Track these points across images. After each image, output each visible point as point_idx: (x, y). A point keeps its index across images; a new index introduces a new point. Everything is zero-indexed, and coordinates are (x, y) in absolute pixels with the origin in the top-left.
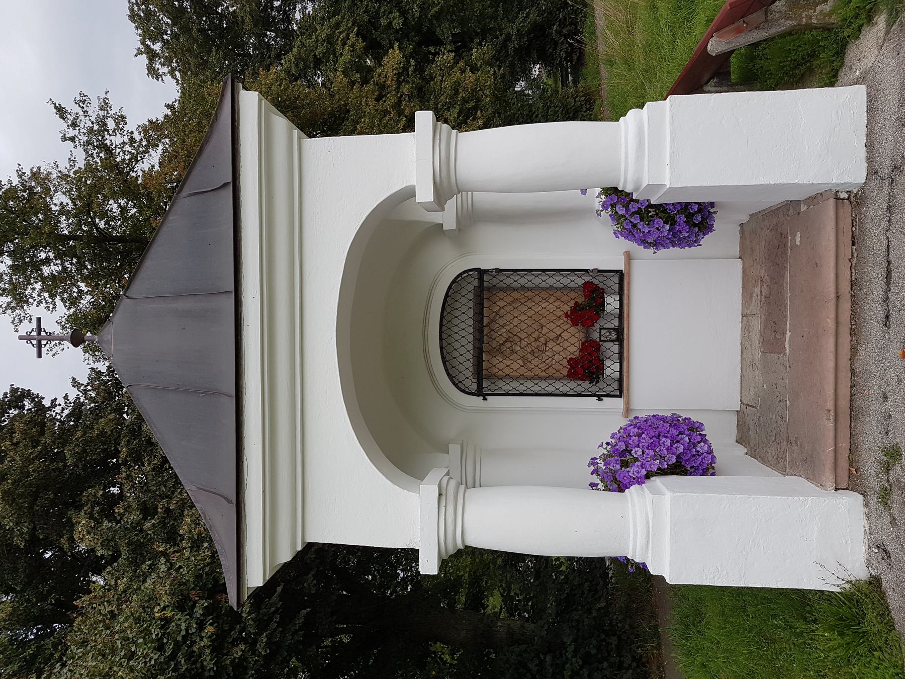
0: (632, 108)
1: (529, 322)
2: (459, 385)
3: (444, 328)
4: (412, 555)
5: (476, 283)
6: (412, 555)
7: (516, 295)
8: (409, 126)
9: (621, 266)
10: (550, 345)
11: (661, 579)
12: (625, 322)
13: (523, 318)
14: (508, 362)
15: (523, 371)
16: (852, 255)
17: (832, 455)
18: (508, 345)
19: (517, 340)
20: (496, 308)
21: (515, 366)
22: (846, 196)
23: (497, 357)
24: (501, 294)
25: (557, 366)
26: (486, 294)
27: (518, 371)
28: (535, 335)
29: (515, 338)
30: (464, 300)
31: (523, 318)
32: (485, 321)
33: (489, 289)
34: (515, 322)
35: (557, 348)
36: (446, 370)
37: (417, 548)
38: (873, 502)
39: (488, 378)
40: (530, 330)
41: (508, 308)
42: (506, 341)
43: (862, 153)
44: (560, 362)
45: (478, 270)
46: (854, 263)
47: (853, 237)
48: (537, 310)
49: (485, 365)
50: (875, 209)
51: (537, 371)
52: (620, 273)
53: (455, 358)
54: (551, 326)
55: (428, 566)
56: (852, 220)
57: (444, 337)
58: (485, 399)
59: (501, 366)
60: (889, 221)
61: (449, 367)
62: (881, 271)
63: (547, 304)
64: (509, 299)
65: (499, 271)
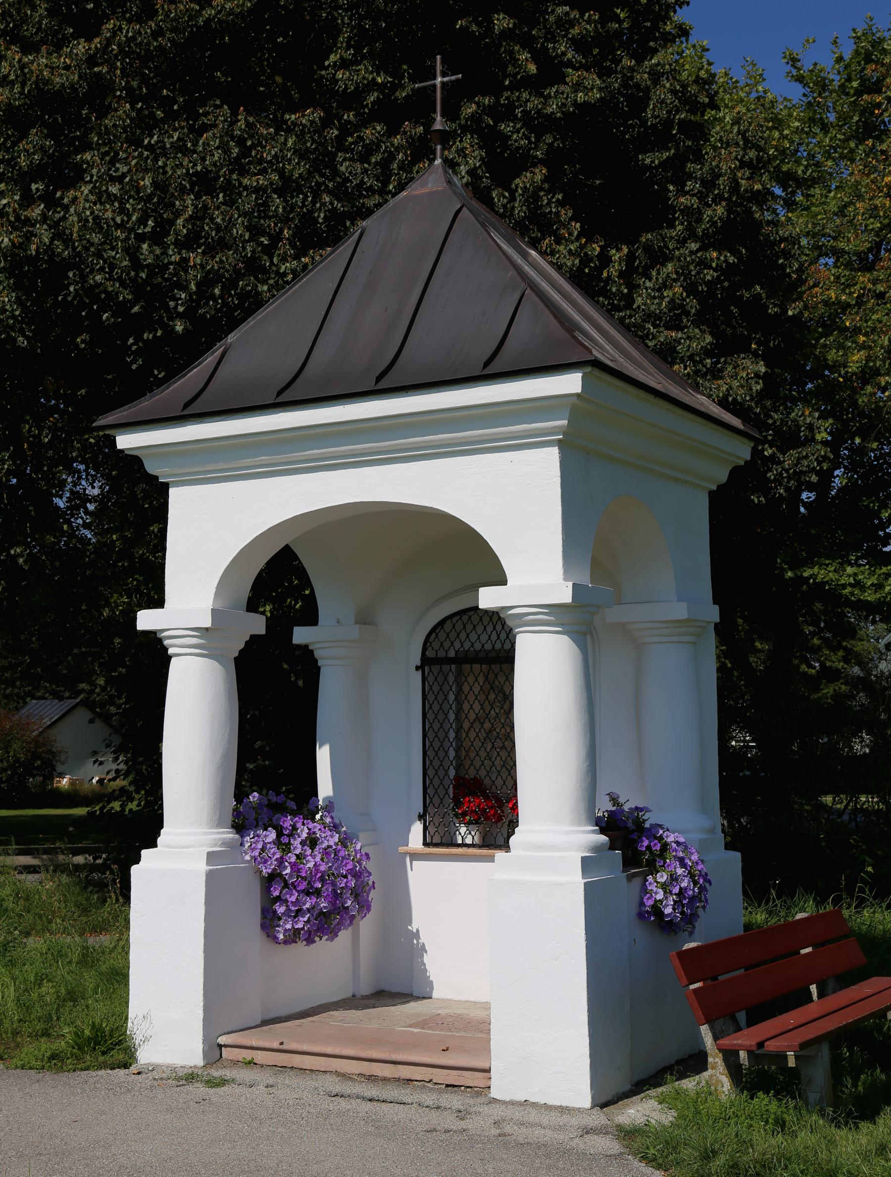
2: (433, 635)
4: (158, 602)
6: (158, 602)
11: (137, 860)
16: (436, 1084)
39: (460, 672)
46: (429, 1085)
47: (454, 1086)
48: (481, 753)
55: (146, 620)
56: (471, 1087)
58: (417, 668)
61: (455, 619)
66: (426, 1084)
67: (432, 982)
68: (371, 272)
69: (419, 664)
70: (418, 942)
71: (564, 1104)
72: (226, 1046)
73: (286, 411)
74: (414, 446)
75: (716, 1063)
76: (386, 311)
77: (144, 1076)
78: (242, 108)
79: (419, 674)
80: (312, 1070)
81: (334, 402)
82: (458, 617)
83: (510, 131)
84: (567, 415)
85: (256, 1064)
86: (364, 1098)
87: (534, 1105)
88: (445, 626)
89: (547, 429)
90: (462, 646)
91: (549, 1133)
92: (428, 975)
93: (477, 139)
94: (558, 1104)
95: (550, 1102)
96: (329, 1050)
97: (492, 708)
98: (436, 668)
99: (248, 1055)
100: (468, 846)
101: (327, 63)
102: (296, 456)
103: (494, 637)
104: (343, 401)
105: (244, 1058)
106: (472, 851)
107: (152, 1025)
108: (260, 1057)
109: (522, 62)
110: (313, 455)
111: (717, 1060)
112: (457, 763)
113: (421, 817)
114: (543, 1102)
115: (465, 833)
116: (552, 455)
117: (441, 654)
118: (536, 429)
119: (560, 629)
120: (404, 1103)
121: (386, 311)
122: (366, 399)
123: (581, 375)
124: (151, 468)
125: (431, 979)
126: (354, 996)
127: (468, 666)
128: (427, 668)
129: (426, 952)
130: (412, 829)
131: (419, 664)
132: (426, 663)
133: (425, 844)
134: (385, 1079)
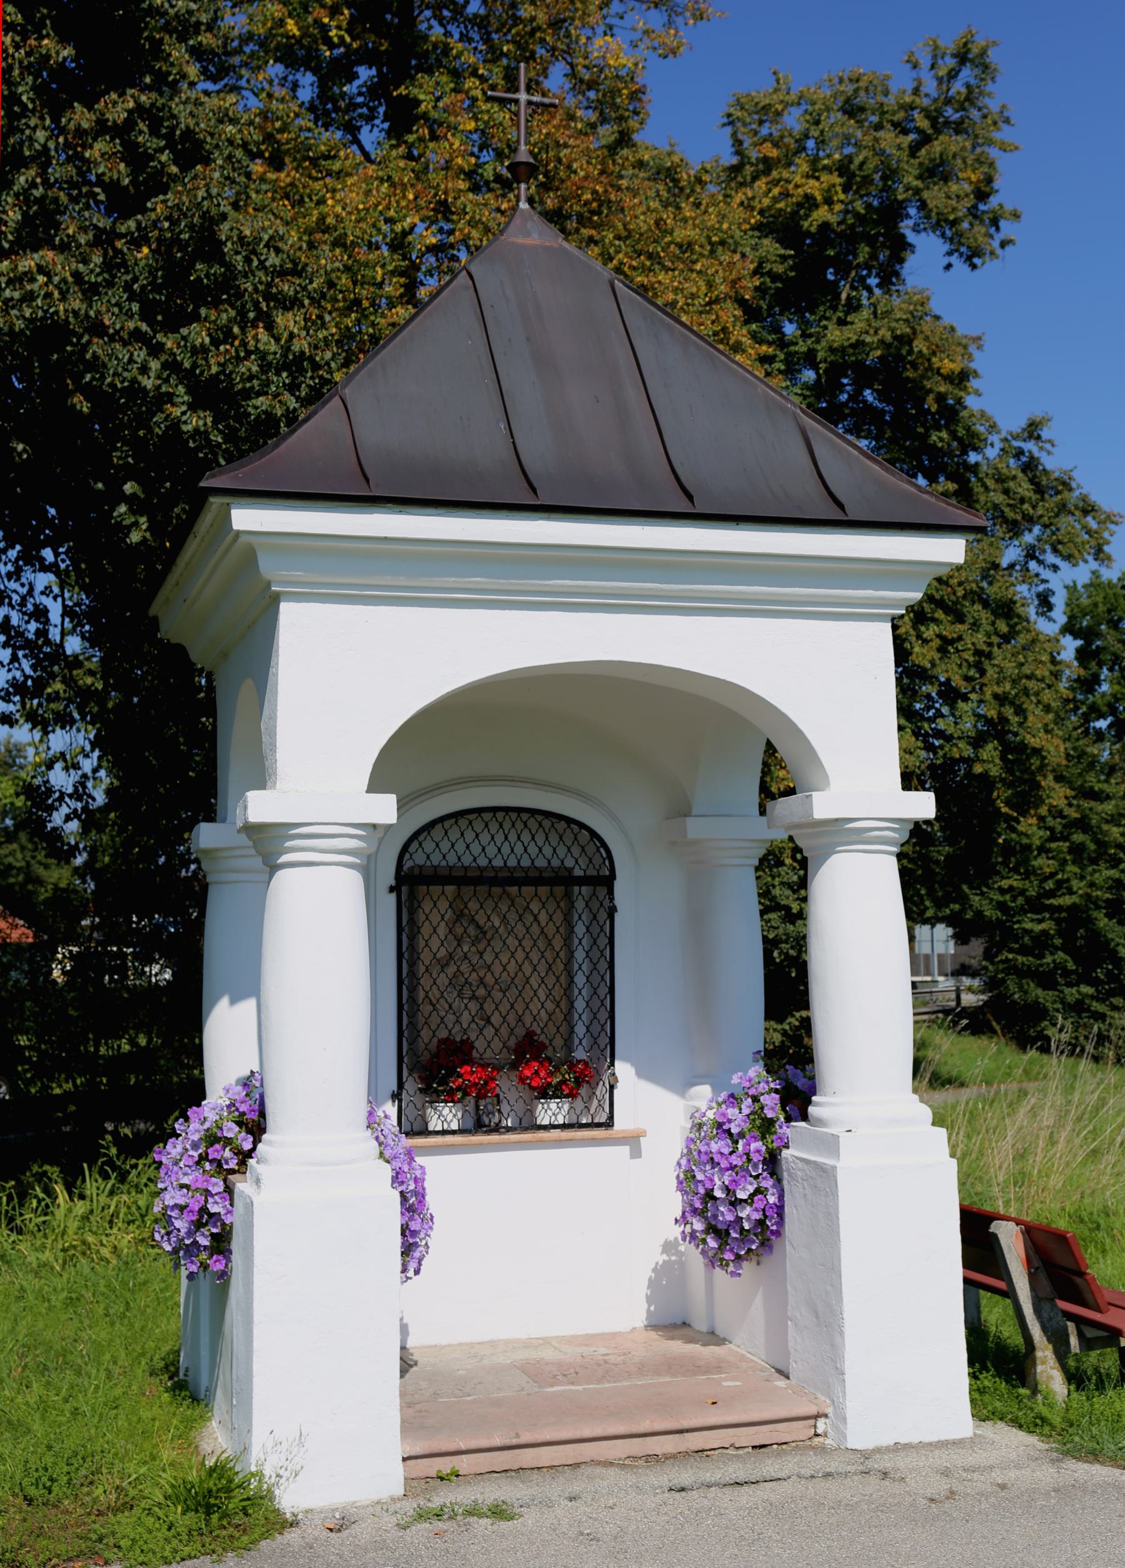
0: (930, 1106)
1: (512, 967)
2: (415, 845)
3: (514, 815)
5: (578, 872)
7: (558, 943)
8: (910, 780)
9: (619, 1123)
10: (473, 1006)
12: (530, 1135)
13: (520, 955)
14: (442, 930)
15: (426, 957)
17: (452, 1447)
18: (472, 931)
19: (481, 947)
20: (535, 907)
21: (435, 944)
22: (819, 1431)
23: (449, 911)
24: (558, 917)
25: (434, 1020)
26: (559, 890)
27: (426, 949)
28: (489, 979)
29: (484, 942)
30: (562, 851)
31: (520, 955)
32: (514, 890)
33: (568, 895)
34: (512, 942)
35: (466, 1018)
36: (441, 820)
37: (278, 785)
38: (410, 1506)
40: (497, 969)
41: (535, 930)
42: (478, 927)
43: (887, 1441)
44: (442, 1025)
45: (613, 876)
49: (436, 889)
50: (814, 1463)
51: (426, 982)
52: (609, 1123)
53: (462, 834)
54: (504, 1007)
57: (522, 815)
59: (435, 918)
60: (813, 1477)
61: (447, 824)
62: (741, 1476)
63: (543, 998)
64: (550, 930)
65: (612, 912)
71: (943, 1438)
73: (548, 519)
74: (582, 590)
79: (393, 897)
81: (762, 527)
82: (453, 821)
87: (908, 1446)
88: (433, 833)
89: (895, 599)
93: (121, 145)
96: (587, 1433)
99: (444, 1465)
100: (453, 1132)
103: (506, 849)
104: (561, 516)
106: (555, 1134)
108: (464, 1464)
110: (562, 586)
112: (572, 1017)
113: (396, 1096)
117: (591, 872)
118: (881, 598)
119: (363, 833)
122: (798, 529)
127: (576, 889)
128: (404, 889)
131: (393, 883)
134: (669, 1457)
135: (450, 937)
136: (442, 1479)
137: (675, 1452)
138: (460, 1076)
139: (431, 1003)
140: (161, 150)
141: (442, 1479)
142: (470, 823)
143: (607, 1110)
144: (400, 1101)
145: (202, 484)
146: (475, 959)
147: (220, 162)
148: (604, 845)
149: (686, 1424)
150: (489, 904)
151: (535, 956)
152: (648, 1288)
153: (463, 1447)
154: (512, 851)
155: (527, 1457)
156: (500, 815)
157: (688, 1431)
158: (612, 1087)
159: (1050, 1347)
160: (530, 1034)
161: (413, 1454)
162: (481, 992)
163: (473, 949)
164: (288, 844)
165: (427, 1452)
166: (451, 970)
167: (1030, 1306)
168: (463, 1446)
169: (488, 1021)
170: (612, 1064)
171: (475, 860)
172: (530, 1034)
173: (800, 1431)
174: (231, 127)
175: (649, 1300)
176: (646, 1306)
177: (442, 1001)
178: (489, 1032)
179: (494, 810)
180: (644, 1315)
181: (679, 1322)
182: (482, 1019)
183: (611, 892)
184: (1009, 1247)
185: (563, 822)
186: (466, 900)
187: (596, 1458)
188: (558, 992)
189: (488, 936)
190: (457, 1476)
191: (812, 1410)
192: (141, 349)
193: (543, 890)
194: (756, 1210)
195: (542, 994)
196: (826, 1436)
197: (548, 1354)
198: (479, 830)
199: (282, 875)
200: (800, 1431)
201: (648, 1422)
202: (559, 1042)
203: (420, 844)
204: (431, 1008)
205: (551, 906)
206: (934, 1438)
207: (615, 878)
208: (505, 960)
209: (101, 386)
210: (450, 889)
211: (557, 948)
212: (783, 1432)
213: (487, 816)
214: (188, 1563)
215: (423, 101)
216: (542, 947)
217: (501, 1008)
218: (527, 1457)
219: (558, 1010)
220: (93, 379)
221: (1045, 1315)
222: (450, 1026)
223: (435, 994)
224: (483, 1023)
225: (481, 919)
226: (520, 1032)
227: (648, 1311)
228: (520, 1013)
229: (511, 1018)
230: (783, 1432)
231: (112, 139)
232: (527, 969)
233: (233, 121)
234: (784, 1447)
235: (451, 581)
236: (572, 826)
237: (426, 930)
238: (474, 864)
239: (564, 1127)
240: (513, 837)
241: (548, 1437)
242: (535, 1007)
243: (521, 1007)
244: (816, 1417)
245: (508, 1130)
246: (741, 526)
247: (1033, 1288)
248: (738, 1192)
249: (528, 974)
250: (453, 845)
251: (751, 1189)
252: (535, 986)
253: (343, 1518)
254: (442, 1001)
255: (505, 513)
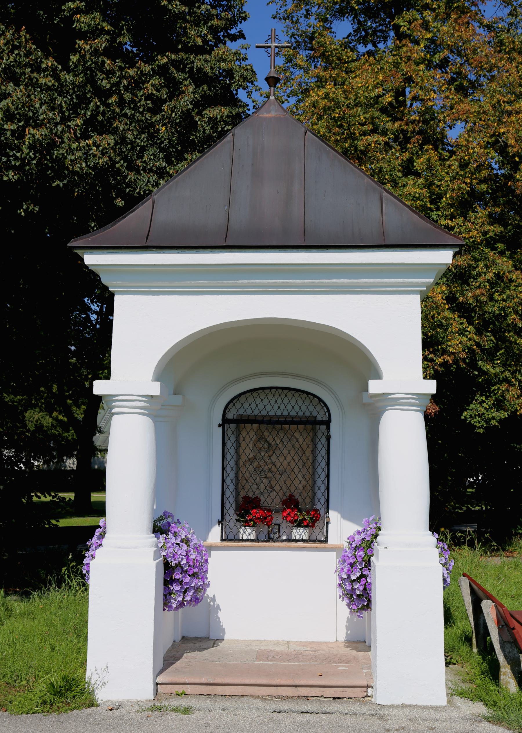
1: (285, 464)
2: (232, 404)
3: (280, 391)
5: (319, 418)
7: (308, 452)
10: (266, 481)
13: (289, 458)
14: (251, 445)
15: (243, 458)
17: (182, 681)
19: (270, 453)
20: (297, 435)
22: (369, 694)
23: (255, 437)
24: (308, 440)
25: (247, 487)
26: (309, 427)
28: (274, 469)
30: (311, 408)
31: (289, 458)
32: (287, 426)
34: (285, 452)
35: (262, 487)
36: (244, 393)
45: (329, 420)
47: (339, 698)
49: (249, 426)
52: (326, 541)
54: (281, 482)
59: (248, 440)
60: (347, 714)
61: (247, 395)
63: (300, 478)
64: (305, 446)
66: (318, 698)
67: (224, 629)
68: (252, 165)
69: (221, 423)
70: (214, 604)
71: (429, 704)
72: (161, 684)
73: (231, 252)
75: (506, 671)
76: (278, 193)
77: (113, 711)
78: (24, 27)
80: (231, 696)
82: (250, 393)
83: (181, 78)
84: (434, 275)
85: (186, 694)
86: (297, 712)
89: (418, 283)
90: (253, 412)
91: (448, 724)
92: (221, 624)
93: (164, 80)
94: (425, 704)
95: (420, 704)
96: (247, 682)
97: (274, 452)
98: (233, 426)
99: (180, 689)
101: (63, 7)
102: (202, 283)
103: (276, 407)
105: (177, 691)
106: (301, 544)
107: (108, 674)
108: (189, 689)
109: (192, 35)
111: (507, 669)
113: (220, 522)
114: (414, 704)
115: (247, 532)
116: (416, 300)
118: (410, 283)
120: (329, 713)
121: (278, 193)
122: (359, 250)
123: (452, 252)
124: (105, 281)
125: (223, 627)
126: (174, 642)
129: (220, 610)
130: (212, 530)
131: (221, 423)
132: (225, 422)
133: (222, 540)
134: (288, 698)
135: (255, 448)
136: (178, 695)
137: (292, 695)
138: (251, 514)
139: (246, 479)
140: (186, 79)
141: (178, 695)
142: (259, 394)
143: (325, 534)
144: (222, 525)
145: (69, 245)
146: (266, 459)
147: (237, 78)
148: (326, 405)
149: (297, 683)
150: (274, 433)
151: (296, 459)
152: (347, 622)
153: (187, 682)
154: (279, 408)
155: (219, 690)
156: (273, 391)
157: (299, 686)
158: (327, 523)
159: (509, 667)
160: (291, 496)
161: (163, 682)
162: (270, 475)
163: (266, 454)
164: (114, 404)
165: (170, 682)
166: (256, 464)
167: (499, 645)
168: (187, 681)
169: (273, 488)
170: (328, 512)
171: (260, 412)
172: (291, 496)
173: (359, 693)
174: (223, 63)
175: (347, 628)
176: (346, 631)
177: (251, 478)
178: (274, 494)
179: (271, 388)
180: (345, 635)
181: (362, 641)
182: (270, 488)
183: (328, 428)
184: (488, 613)
185: (305, 394)
186: (263, 431)
187: (252, 694)
188: (308, 476)
189: (274, 448)
190: (186, 694)
191: (365, 683)
192: (154, 175)
193: (301, 427)
194: (361, 585)
195: (300, 476)
196: (372, 697)
197: (278, 648)
198: (262, 398)
199: (115, 418)
200: (359, 693)
201: (279, 680)
202: (308, 500)
203: (234, 405)
204: (245, 481)
205: (305, 435)
206: (425, 704)
207: (331, 422)
208: (281, 460)
209: (133, 194)
210: (255, 426)
211: (308, 455)
212: (349, 693)
213: (267, 391)
214: (35, 715)
215: (401, 26)
216: (300, 454)
217: (279, 482)
218: (219, 690)
219: (308, 485)
220: (130, 191)
221: (507, 650)
222: (254, 490)
223: (247, 475)
224: (271, 490)
225: (270, 439)
226: (288, 494)
227: (347, 633)
228: (289, 485)
229: (284, 488)
230: (349, 693)
231: (160, 78)
232: (293, 464)
233: (224, 60)
234: (350, 700)
235: (190, 283)
236: (309, 396)
237: (243, 445)
238: (260, 414)
239: (303, 541)
240: (279, 401)
241: (228, 681)
242: (296, 482)
243: (288, 483)
244: (367, 687)
245: (284, 541)
246: (329, 250)
247: (500, 635)
248: (351, 576)
249: (293, 467)
250: (250, 405)
251: (358, 575)
252: (296, 472)
253: (120, 706)
254: (251, 478)
255: (209, 250)
